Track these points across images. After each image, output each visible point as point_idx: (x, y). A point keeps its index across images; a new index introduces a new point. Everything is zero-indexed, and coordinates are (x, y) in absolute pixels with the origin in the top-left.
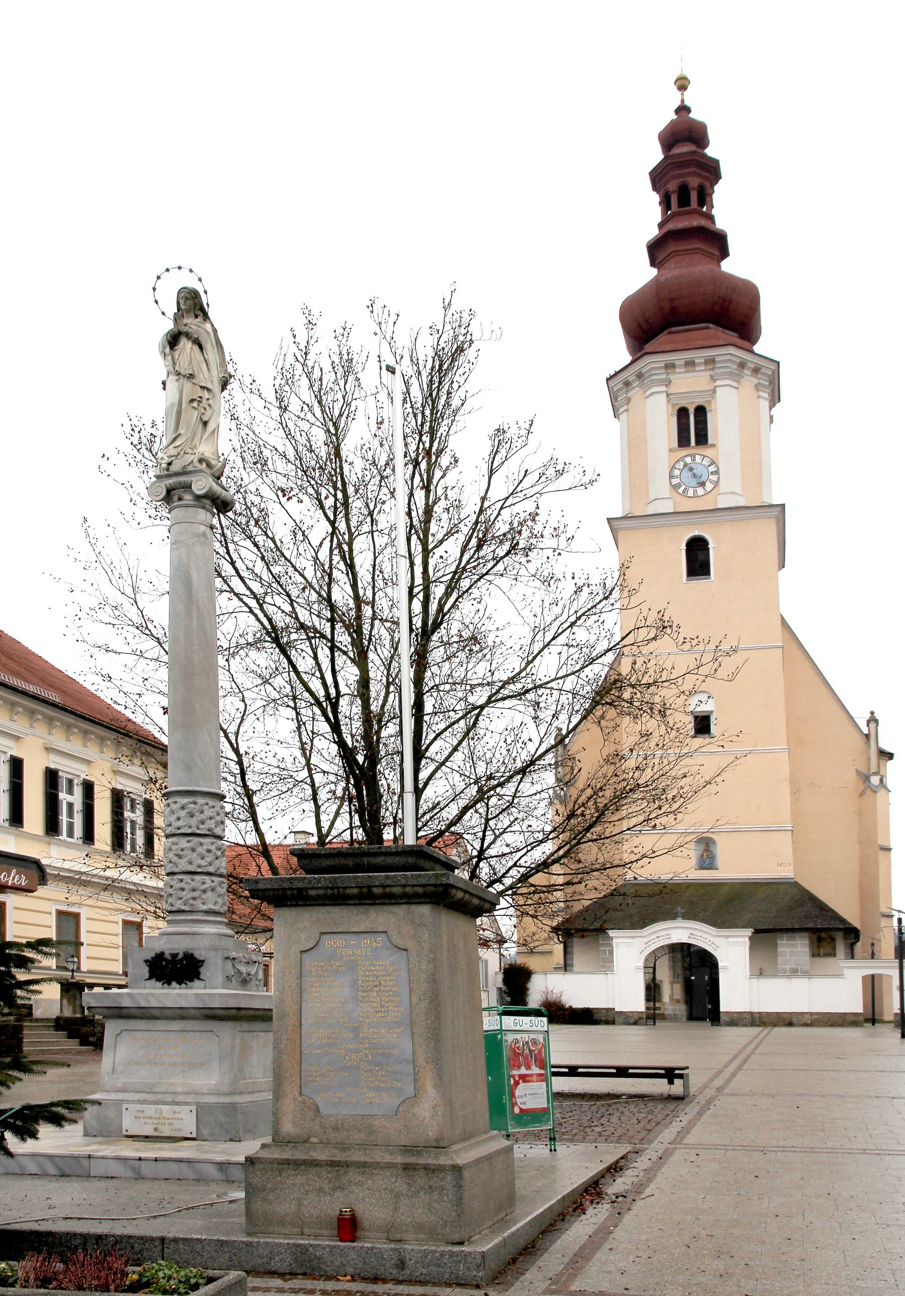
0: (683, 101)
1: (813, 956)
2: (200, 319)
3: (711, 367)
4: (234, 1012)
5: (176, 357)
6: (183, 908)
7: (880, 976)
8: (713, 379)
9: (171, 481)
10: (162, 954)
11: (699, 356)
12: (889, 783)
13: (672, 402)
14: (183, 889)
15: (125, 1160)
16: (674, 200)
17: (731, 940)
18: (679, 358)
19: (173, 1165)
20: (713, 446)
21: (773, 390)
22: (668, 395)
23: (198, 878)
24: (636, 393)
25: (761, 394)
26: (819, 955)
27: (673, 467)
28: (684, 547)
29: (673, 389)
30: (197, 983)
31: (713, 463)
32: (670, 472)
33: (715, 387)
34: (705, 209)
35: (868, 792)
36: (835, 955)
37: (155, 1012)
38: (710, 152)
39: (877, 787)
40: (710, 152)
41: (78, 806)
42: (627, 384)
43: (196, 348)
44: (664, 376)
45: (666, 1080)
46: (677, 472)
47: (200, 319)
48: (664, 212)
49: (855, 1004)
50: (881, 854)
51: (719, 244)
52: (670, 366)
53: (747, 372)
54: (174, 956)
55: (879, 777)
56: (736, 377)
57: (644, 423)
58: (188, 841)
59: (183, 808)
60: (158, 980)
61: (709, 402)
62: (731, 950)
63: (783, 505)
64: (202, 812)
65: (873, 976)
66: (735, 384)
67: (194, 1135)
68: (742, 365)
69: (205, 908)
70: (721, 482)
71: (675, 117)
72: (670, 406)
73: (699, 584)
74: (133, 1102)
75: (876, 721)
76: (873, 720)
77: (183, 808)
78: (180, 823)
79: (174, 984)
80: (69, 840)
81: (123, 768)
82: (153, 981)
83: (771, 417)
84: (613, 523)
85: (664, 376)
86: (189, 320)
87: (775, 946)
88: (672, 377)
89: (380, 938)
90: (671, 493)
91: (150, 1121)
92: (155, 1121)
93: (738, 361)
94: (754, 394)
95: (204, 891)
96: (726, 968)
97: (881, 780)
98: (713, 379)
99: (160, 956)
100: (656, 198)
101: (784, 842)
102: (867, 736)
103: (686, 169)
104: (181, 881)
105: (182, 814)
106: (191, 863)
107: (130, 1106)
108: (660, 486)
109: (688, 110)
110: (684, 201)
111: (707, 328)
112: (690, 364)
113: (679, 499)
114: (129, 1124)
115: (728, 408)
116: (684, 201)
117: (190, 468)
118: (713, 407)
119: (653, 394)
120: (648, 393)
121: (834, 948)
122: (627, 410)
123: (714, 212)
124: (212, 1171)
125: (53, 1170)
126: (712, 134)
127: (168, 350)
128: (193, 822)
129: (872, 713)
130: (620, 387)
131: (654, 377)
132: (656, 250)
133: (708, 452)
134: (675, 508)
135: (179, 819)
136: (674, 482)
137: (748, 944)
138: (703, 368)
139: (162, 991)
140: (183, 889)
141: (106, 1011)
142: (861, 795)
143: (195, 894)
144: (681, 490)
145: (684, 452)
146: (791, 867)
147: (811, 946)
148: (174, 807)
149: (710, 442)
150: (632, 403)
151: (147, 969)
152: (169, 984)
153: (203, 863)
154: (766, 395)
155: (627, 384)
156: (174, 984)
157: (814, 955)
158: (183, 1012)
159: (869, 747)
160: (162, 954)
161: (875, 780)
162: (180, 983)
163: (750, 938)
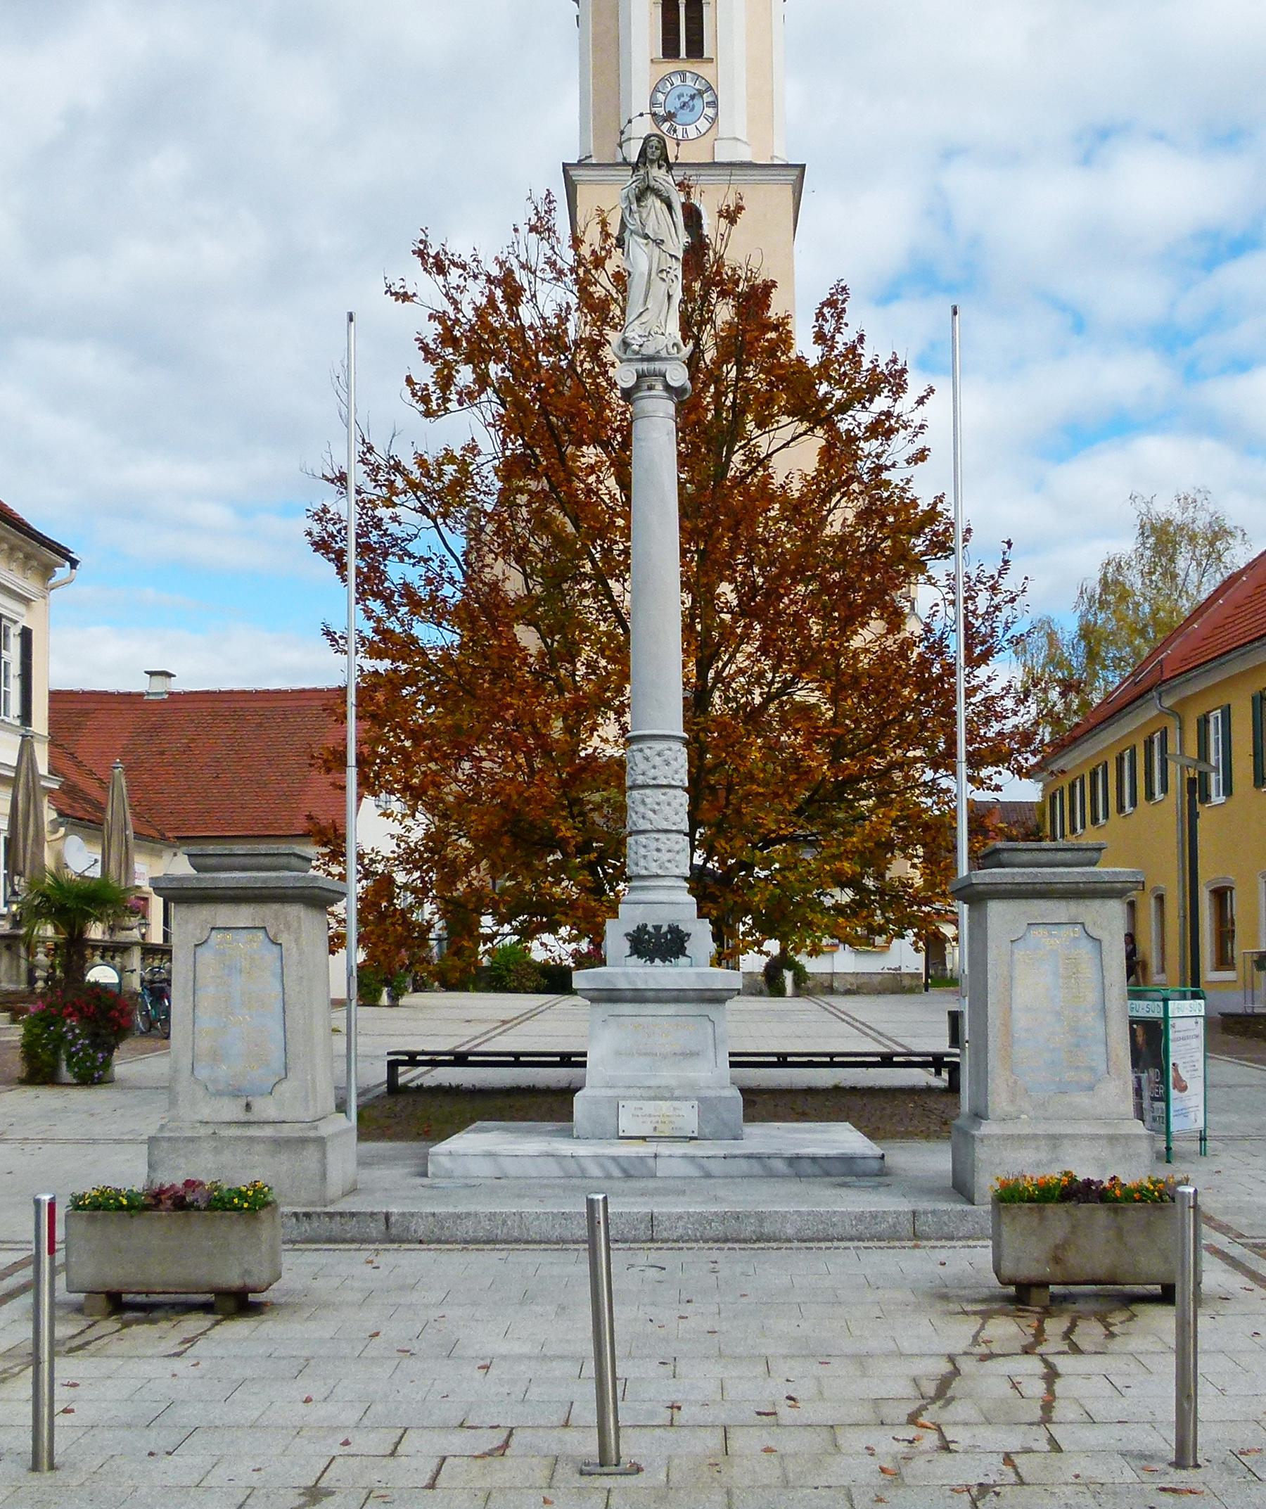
4: (675, 993)
5: (644, 216)
6: (660, 872)
9: (645, 366)
15: (692, 1158)
19: (743, 1162)
20: (711, 60)
30: (682, 960)
43: (664, 207)
54: (658, 928)
58: (664, 794)
60: (640, 956)
63: (804, 166)
64: (676, 759)
67: (695, 1135)
74: (630, 1098)
78: (652, 773)
79: (657, 961)
89: (1078, 928)
91: (649, 1119)
92: (654, 1119)
95: (678, 852)
99: (642, 929)
104: (657, 840)
106: (666, 820)
107: (627, 1103)
114: (628, 1125)
124: (780, 1166)
125: (616, 1172)
139: (641, 970)
143: (669, 856)
145: (671, 66)
151: (628, 944)
152: (652, 961)
156: (657, 961)
158: (661, 994)
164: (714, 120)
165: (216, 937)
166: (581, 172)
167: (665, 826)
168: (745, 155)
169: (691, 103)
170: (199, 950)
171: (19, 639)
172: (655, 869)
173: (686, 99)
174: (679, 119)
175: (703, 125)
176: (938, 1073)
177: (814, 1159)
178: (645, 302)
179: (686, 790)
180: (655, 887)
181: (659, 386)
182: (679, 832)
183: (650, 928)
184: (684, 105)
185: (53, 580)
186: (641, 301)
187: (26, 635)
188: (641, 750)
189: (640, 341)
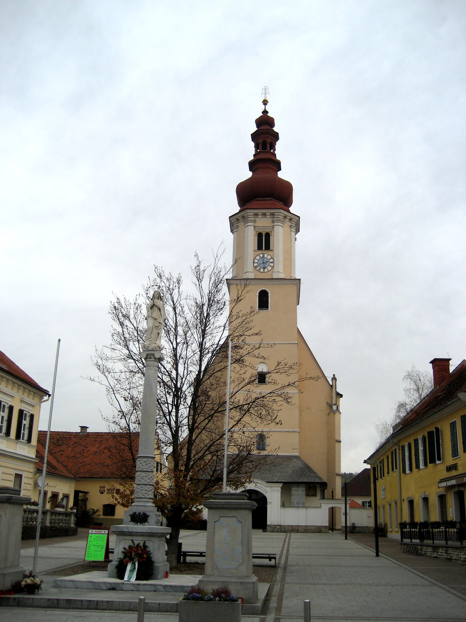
0: (265, 109)
1: (306, 496)
2: (159, 300)
4: (161, 534)
6: (142, 497)
7: (335, 507)
8: (273, 222)
11: (268, 212)
12: (341, 410)
14: (142, 490)
16: (260, 146)
17: (273, 488)
18: (260, 212)
19: (150, 586)
20: (272, 250)
21: (297, 228)
23: (147, 486)
24: (241, 224)
25: (292, 229)
26: (309, 496)
27: (255, 258)
28: (258, 295)
30: (146, 523)
32: (254, 260)
34: (272, 151)
35: (332, 414)
36: (316, 496)
37: (134, 533)
38: (275, 129)
39: (335, 411)
40: (275, 129)
41: (27, 426)
42: (238, 220)
43: (158, 310)
44: (253, 219)
45: (268, 560)
47: (159, 300)
48: (256, 151)
49: (324, 521)
50: (337, 444)
51: (277, 165)
52: (256, 215)
54: (139, 513)
55: (336, 406)
56: (283, 222)
57: (244, 238)
59: (144, 462)
60: (134, 522)
61: (271, 231)
62: (273, 495)
64: (150, 464)
65: (333, 507)
66: (282, 225)
68: (285, 217)
69: (148, 497)
73: (263, 312)
75: (336, 379)
76: (334, 379)
77: (144, 462)
78: (143, 467)
79: (139, 524)
80: (22, 441)
81: (27, 399)
83: (296, 238)
84: (229, 281)
85: (253, 219)
86: (156, 300)
87: (291, 491)
93: (283, 215)
94: (289, 229)
95: (149, 491)
96: (270, 503)
97: (337, 408)
98: (273, 222)
99: (135, 514)
100: (253, 144)
101: (295, 438)
102: (332, 386)
103: (265, 134)
105: (144, 464)
108: (249, 267)
109: (267, 112)
110: (264, 147)
111: (271, 200)
112: (264, 215)
113: (257, 272)
115: (279, 234)
116: (264, 147)
117: (154, 349)
118: (273, 234)
120: (246, 225)
121: (316, 492)
122: (237, 231)
123: (276, 152)
124: (161, 588)
127: (150, 310)
128: (147, 467)
129: (334, 375)
130: (235, 221)
131: (249, 219)
132: (252, 165)
133: (270, 253)
135: (143, 466)
136: (255, 265)
137: (280, 491)
139: (134, 526)
140: (142, 490)
141: (117, 533)
142: (329, 415)
143: (146, 492)
144: (258, 269)
145: (260, 252)
146: (298, 451)
147: (306, 490)
148: (142, 461)
150: (240, 228)
153: (149, 481)
154: (294, 230)
155: (238, 220)
156: (139, 524)
157: (307, 495)
159: (332, 391)
161: (334, 408)
162: (141, 523)
163: (281, 488)
164: (273, 267)
167: (145, 483)
168: (282, 276)
170: (216, 523)
171: (29, 417)
175: (269, 268)
177: (171, 586)
181: (153, 358)
183: (137, 513)
185: (43, 400)
187: (32, 416)
188: (139, 461)
189: (148, 345)
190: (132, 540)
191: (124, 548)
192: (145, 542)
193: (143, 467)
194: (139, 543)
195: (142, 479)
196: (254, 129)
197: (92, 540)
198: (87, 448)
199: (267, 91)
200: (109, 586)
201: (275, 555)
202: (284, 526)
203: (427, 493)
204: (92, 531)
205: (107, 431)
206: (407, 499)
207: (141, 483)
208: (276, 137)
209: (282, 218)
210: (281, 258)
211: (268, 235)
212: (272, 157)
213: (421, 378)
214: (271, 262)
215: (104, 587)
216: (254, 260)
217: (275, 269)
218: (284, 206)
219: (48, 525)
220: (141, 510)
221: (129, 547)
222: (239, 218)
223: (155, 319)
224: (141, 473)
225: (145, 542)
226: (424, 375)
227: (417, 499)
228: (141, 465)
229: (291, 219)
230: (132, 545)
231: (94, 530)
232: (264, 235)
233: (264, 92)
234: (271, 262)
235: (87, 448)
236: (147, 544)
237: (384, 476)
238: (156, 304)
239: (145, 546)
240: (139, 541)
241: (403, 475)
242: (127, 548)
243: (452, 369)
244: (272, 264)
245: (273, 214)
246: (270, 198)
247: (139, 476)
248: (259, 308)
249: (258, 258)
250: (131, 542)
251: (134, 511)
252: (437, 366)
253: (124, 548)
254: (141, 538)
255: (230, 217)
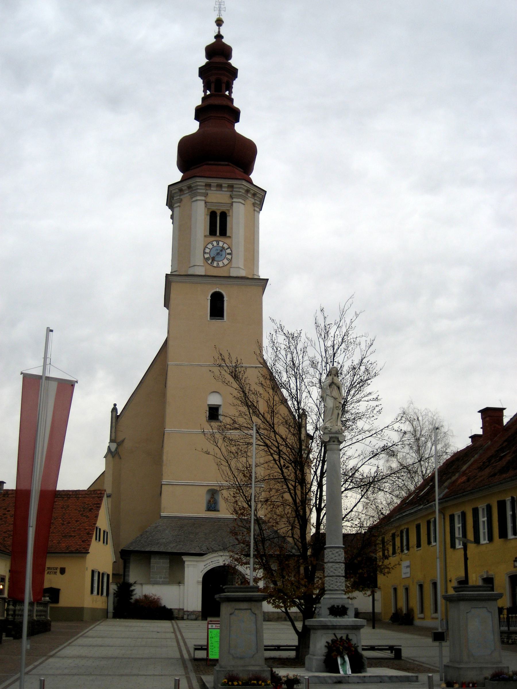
0: (219, 32)
3: (230, 190)
8: (231, 197)
10: (334, 606)
11: (225, 182)
13: (208, 207)
14: (337, 582)
16: (213, 86)
18: (214, 182)
20: (230, 237)
22: (206, 203)
24: (186, 197)
27: (206, 247)
28: (209, 298)
29: (209, 200)
30: (346, 616)
31: (229, 248)
32: (204, 249)
33: (233, 202)
37: (337, 627)
42: (181, 190)
44: (204, 191)
46: (207, 250)
51: (235, 115)
52: (208, 186)
53: (249, 195)
54: (338, 606)
56: (245, 198)
60: (333, 615)
61: (228, 210)
63: (268, 280)
66: (243, 202)
68: (248, 191)
70: (233, 260)
71: (214, 40)
72: (206, 210)
73: (217, 323)
78: (335, 558)
79: (338, 617)
82: (331, 616)
88: (209, 192)
90: (204, 263)
93: (246, 188)
98: (231, 197)
99: (333, 606)
103: (218, 69)
105: (337, 555)
111: (228, 165)
112: (220, 186)
113: (209, 267)
115: (238, 213)
119: (197, 200)
120: (194, 199)
122: (179, 206)
123: (233, 96)
124: (387, 679)
126: (234, 53)
131: (199, 191)
132: (200, 113)
133: (227, 240)
134: (206, 273)
138: (226, 190)
143: (340, 584)
145: (212, 239)
149: (228, 234)
156: (338, 617)
160: (334, 606)
164: (230, 261)
165: (237, 612)
166: (172, 278)
168: (243, 273)
169: (221, 253)
172: (336, 588)
173: (219, 251)
174: (216, 259)
175: (226, 262)
176: (392, 652)
178: (332, 415)
179: (344, 563)
180: (336, 594)
181: (336, 441)
182: (342, 576)
183: (336, 606)
184: (218, 254)
186: (330, 414)
190: (334, 634)
191: (327, 642)
192: (347, 636)
193: (335, 558)
194: (342, 637)
195: (335, 570)
196: (203, 61)
197: (213, 636)
198: (9, 511)
199: (222, 6)
200: (335, 680)
201: (401, 646)
202: (268, 612)
203: (491, 573)
204: (212, 626)
205: (163, 506)
206: (456, 579)
207: (334, 575)
208: (233, 73)
209: (243, 191)
210: (242, 248)
211: (224, 216)
212: (228, 103)
213: (420, 418)
214: (228, 254)
215: (330, 681)
216: (204, 249)
217: (234, 264)
218: (243, 174)
219: (35, 618)
220: (338, 603)
221: (332, 640)
222: (184, 188)
223: (335, 399)
224: (334, 564)
225: (347, 636)
226: (424, 413)
227: (474, 579)
228: (333, 556)
229: (254, 195)
230: (335, 638)
231: (214, 625)
232: (218, 214)
233: (217, 6)
234: (228, 254)
235: (9, 511)
236: (350, 637)
237: (408, 549)
238: (334, 381)
239: (348, 640)
240: (341, 634)
241: (449, 550)
242: (330, 642)
243: (506, 420)
244: (229, 257)
245: (231, 187)
246: (226, 163)
247: (332, 567)
248: (211, 316)
249: (210, 246)
250: (333, 635)
251: (333, 604)
252: (489, 416)
253: (327, 642)
254: (343, 631)
255: (169, 186)
